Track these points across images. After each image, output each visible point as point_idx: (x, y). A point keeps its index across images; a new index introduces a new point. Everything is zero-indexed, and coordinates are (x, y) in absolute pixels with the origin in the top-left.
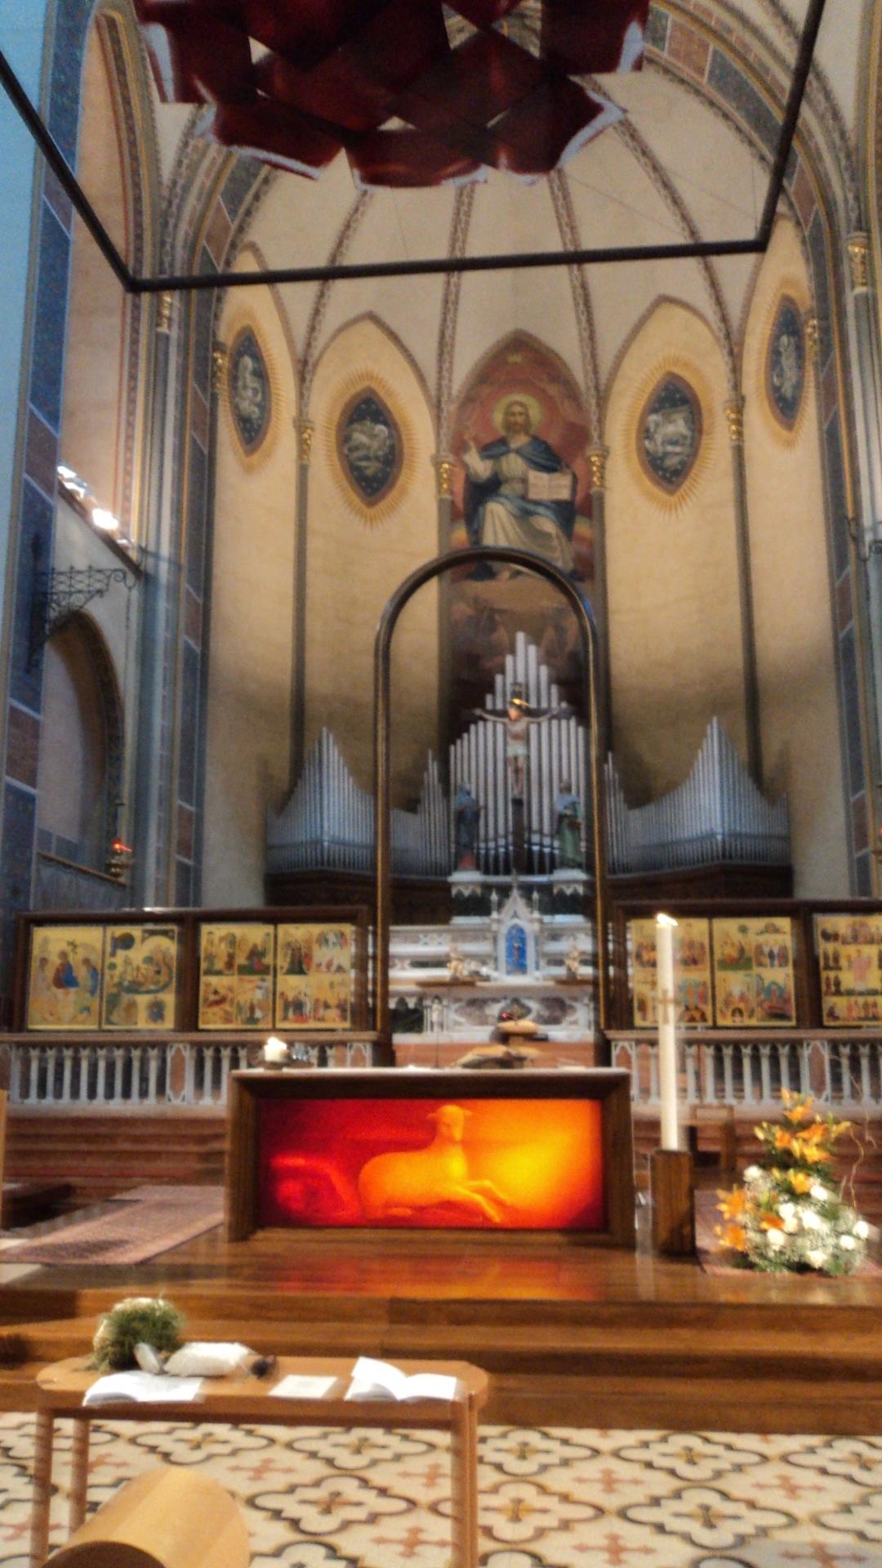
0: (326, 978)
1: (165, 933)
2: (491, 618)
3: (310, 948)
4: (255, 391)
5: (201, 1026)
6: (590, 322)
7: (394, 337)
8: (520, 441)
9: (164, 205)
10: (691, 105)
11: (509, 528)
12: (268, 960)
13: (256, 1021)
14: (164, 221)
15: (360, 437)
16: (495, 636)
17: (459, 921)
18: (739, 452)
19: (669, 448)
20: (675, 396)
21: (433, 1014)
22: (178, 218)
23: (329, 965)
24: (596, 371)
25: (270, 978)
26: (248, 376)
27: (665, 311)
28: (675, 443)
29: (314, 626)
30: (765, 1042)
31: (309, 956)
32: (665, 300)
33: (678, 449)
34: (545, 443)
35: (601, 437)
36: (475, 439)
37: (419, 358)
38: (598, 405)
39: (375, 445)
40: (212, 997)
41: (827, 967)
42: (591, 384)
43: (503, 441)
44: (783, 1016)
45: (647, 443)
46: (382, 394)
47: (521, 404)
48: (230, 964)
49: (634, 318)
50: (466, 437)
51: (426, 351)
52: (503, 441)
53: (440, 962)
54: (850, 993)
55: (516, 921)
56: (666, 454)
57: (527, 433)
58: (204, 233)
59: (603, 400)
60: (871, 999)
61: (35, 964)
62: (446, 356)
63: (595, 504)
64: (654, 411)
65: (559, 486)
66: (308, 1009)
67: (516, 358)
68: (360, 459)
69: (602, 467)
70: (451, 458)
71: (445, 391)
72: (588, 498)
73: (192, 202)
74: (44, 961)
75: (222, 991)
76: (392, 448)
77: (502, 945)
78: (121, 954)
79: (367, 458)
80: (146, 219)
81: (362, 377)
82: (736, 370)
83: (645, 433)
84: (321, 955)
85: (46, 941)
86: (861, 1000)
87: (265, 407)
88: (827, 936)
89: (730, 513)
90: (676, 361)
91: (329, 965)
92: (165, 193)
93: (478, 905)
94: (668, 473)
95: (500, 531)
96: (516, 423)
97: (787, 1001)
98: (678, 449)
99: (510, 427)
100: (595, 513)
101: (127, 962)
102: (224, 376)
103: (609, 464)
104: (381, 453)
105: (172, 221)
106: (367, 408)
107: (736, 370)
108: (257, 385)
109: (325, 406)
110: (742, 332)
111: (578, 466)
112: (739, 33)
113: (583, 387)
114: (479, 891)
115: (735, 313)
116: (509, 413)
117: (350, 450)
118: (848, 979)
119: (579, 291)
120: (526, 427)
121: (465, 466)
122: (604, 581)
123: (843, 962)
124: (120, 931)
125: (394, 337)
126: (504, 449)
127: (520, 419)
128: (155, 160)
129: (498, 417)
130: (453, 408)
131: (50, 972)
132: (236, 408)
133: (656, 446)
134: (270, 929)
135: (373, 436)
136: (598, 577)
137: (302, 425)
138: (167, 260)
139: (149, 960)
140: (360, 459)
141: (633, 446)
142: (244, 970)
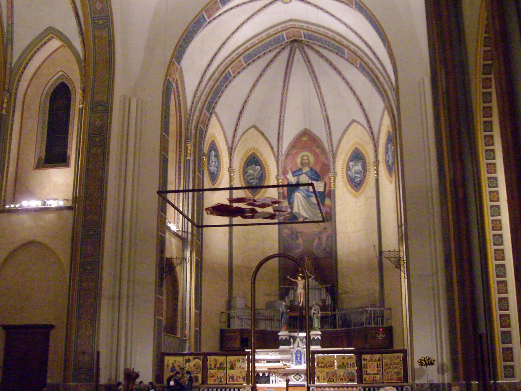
0: (240, 370)
1: (199, 358)
2: (297, 235)
3: (235, 362)
4: (216, 162)
5: (208, 383)
6: (329, 128)
7: (263, 134)
8: (306, 169)
9: (188, 117)
10: (355, 70)
11: (303, 201)
12: (225, 365)
13: (222, 382)
14: (188, 122)
15: (250, 171)
16: (298, 242)
17: (281, 348)
18: (377, 180)
19: (357, 175)
20: (357, 156)
21: (273, 378)
22: (192, 120)
23: (240, 367)
24: (332, 146)
25: (225, 370)
26: (213, 158)
27: (354, 125)
28: (358, 174)
29: (235, 242)
30: (372, 387)
31: (235, 365)
32: (354, 121)
33: (359, 176)
34: (315, 170)
35: (334, 169)
36: (291, 170)
37: (270, 139)
38: (333, 157)
39: (256, 174)
40: (211, 375)
41: (364, 368)
42: (331, 150)
43: (300, 170)
44: (352, 380)
45: (349, 172)
46: (258, 155)
47: (305, 155)
48: (215, 367)
49: (344, 128)
50: (288, 168)
51: (274, 141)
52: (300, 170)
53: (278, 361)
54: (370, 374)
55: (298, 348)
56: (356, 177)
57: (309, 167)
58: (200, 122)
59: (334, 156)
60: (374, 376)
61: (165, 367)
62: (280, 140)
63: (332, 194)
64: (352, 161)
65: (320, 187)
66: (235, 378)
67: (304, 139)
68: (250, 179)
69: (334, 181)
70: (282, 177)
71: (280, 153)
72: (330, 191)
73: (197, 114)
74: (168, 366)
75: (213, 374)
76: (262, 174)
77: (294, 356)
78: (188, 364)
79: (253, 179)
80: (183, 124)
81: (251, 150)
82: (376, 151)
83: (348, 169)
84: (238, 365)
85: (168, 360)
86: (372, 376)
87: (218, 168)
88: (364, 360)
89: (374, 201)
90: (359, 144)
91: (240, 367)
92: (189, 113)
93: (287, 342)
94: (356, 184)
95: (299, 201)
96: (305, 163)
97: (354, 377)
98: (359, 176)
99: (302, 164)
100: (332, 196)
101: (189, 366)
102: (206, 164)
103: (337, 178)
104: (258, 176)
105: (191, 122)
106: (253, 160)
107: (376, 151)
108: (216, 160)
109: (238, 163)
110: (378, 138)
111: (326, 179)
112: (365, 59)
113: (328, 151)
114: (288, 338)
115: (375, 131)
116: (302, 159)
117: (247, 176)
118: (369, 371)
119: (325, 118)
120: (308, 165)
121: (287, 179)
122: (335, 221)
123: (368, 367)
124: (187, 357)
125: (263, 134)
126: (301, 172)
127: (307, 161)
128: (185, 103)
129: (299, 161)
130: (283, 158)
131: (170, 368)
132: (209, 170)
133: (352, 173)
134: (225, 357)
135: (255, 171)
136: (333, 221)
137: (231, 170)
138: (189, 134)
139: (194, 365)
140: (250, 179)
141: (345, 174)
142: (219, 368)
